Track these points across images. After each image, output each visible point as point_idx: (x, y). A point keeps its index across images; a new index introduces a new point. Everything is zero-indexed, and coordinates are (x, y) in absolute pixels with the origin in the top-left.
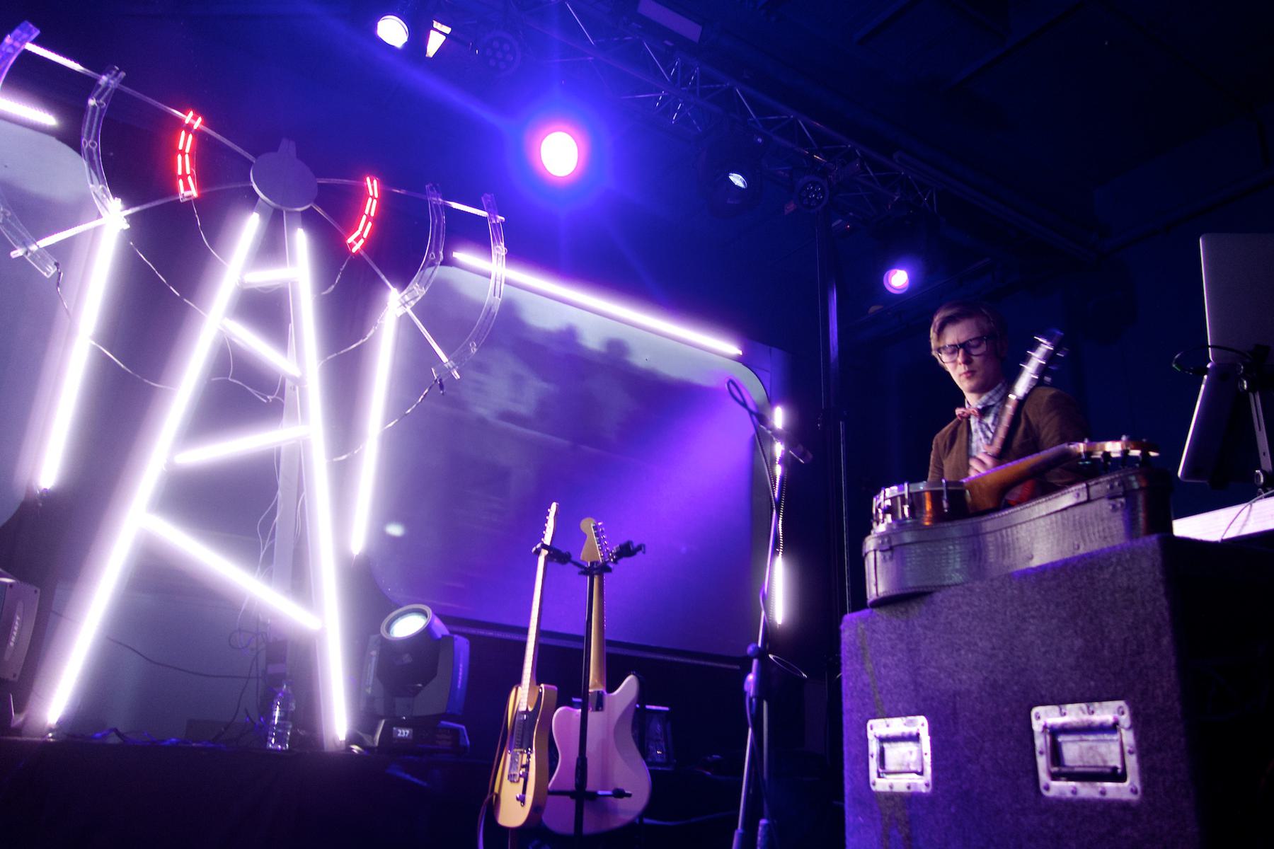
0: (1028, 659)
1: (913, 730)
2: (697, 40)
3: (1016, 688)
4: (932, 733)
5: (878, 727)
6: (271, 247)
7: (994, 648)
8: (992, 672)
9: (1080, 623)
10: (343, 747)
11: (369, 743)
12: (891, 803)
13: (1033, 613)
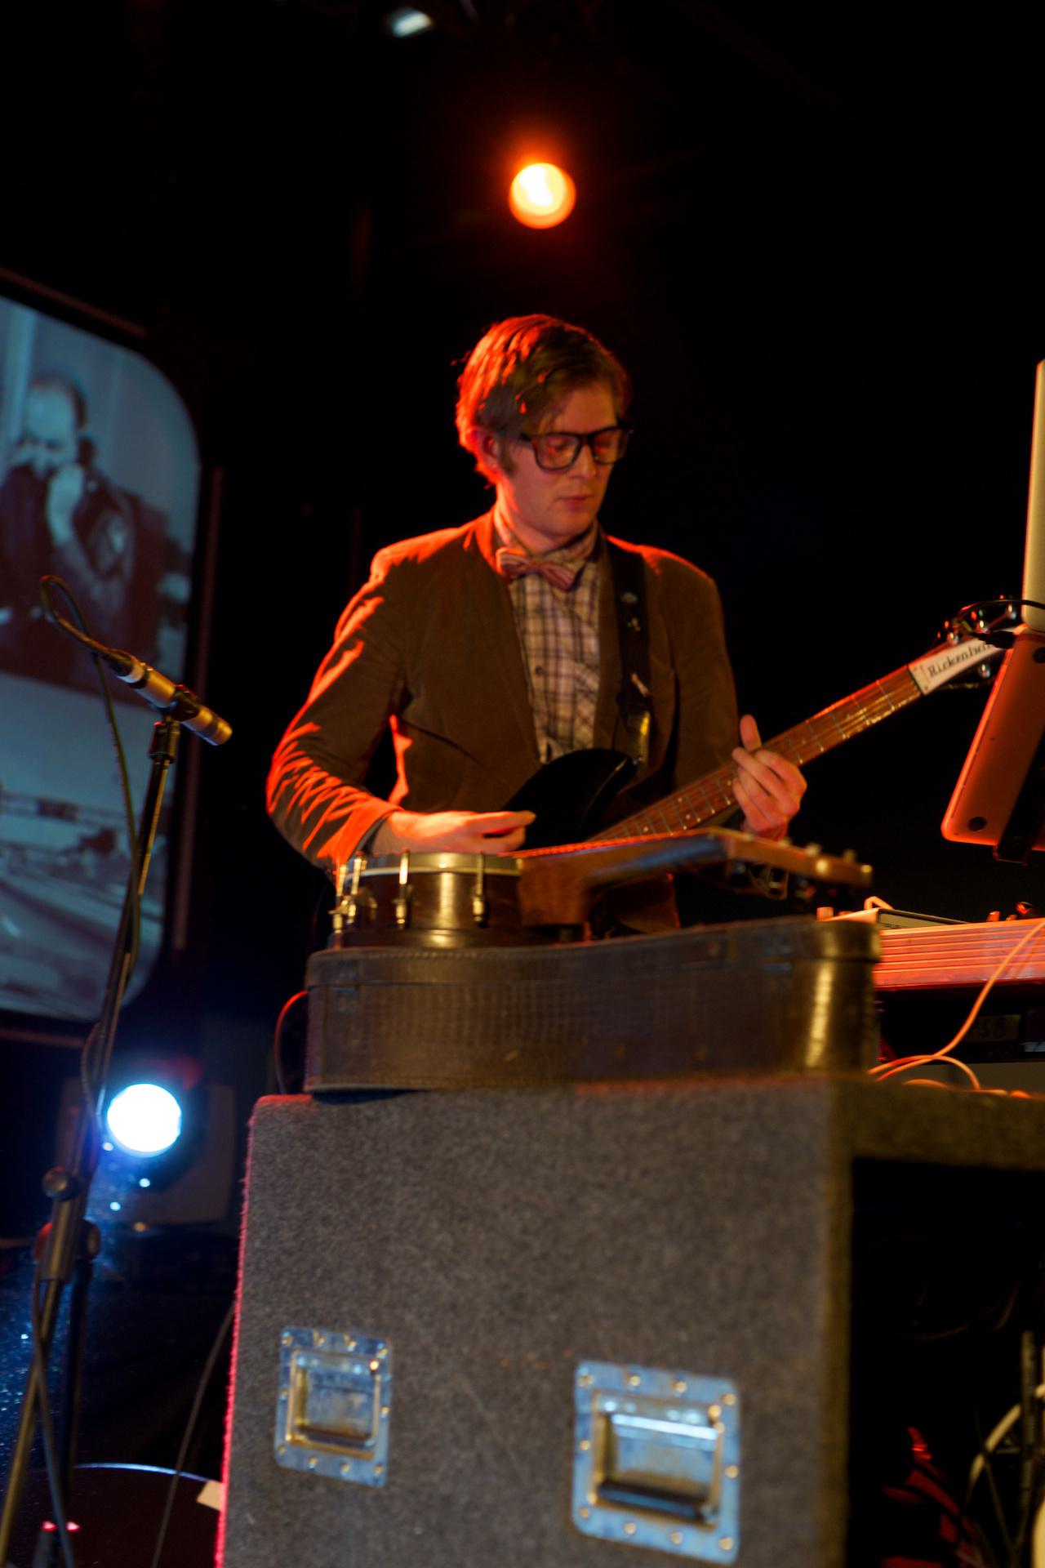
7: (525, 1231)
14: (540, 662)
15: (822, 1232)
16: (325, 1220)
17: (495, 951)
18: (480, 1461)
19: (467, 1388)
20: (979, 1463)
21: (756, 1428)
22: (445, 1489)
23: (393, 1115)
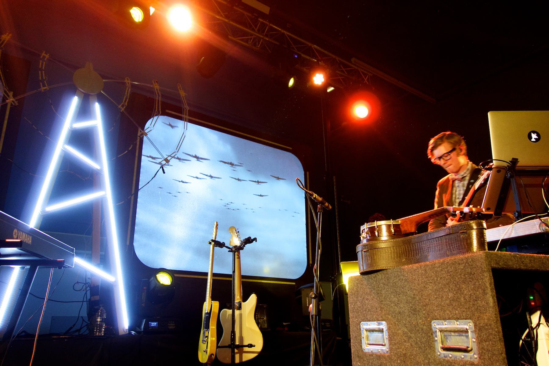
0: (429, 300)
1: (381, 327)
2: (268, 13)
3: (424, 312)
4: (389, 329)
5: (365, 326)
6: (84, 112)
7: (414, 295)
8: (414, 305)
9: (451, 286)
10: (128, 332)
11: (138, 329)
12: (372, 357)
13: (431, 281)
15: (488, 285)
16: (367, 299)
17: (397, 239)
18: (412, 345)
19: (406, 330)
20: (521, 342)
21: (479, 329)
22: (404, 352)
23: (379, 275)
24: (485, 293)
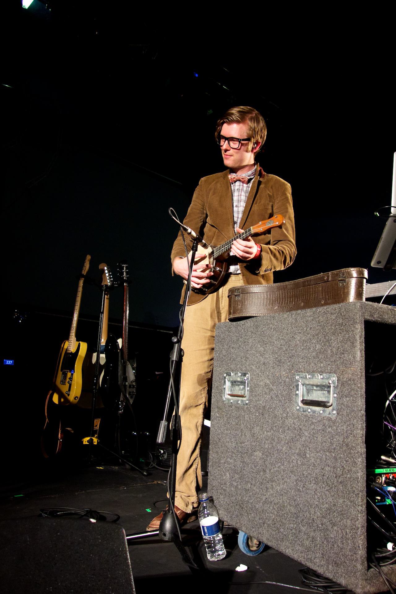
7: (281, 345)
14: (237, 204)
15: (358, 337)
20: (388, 402)
21: (342, 383)
22: (263, 405)
23: (248, 322)
24: (353, 346)
